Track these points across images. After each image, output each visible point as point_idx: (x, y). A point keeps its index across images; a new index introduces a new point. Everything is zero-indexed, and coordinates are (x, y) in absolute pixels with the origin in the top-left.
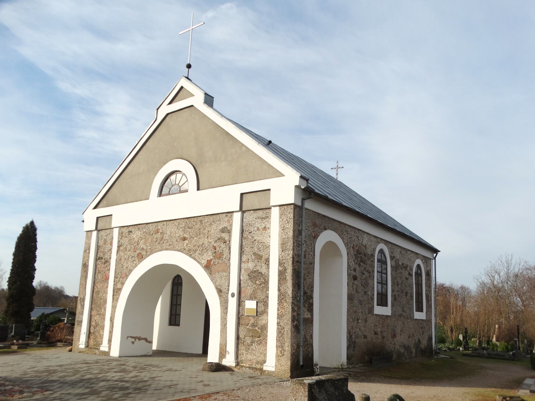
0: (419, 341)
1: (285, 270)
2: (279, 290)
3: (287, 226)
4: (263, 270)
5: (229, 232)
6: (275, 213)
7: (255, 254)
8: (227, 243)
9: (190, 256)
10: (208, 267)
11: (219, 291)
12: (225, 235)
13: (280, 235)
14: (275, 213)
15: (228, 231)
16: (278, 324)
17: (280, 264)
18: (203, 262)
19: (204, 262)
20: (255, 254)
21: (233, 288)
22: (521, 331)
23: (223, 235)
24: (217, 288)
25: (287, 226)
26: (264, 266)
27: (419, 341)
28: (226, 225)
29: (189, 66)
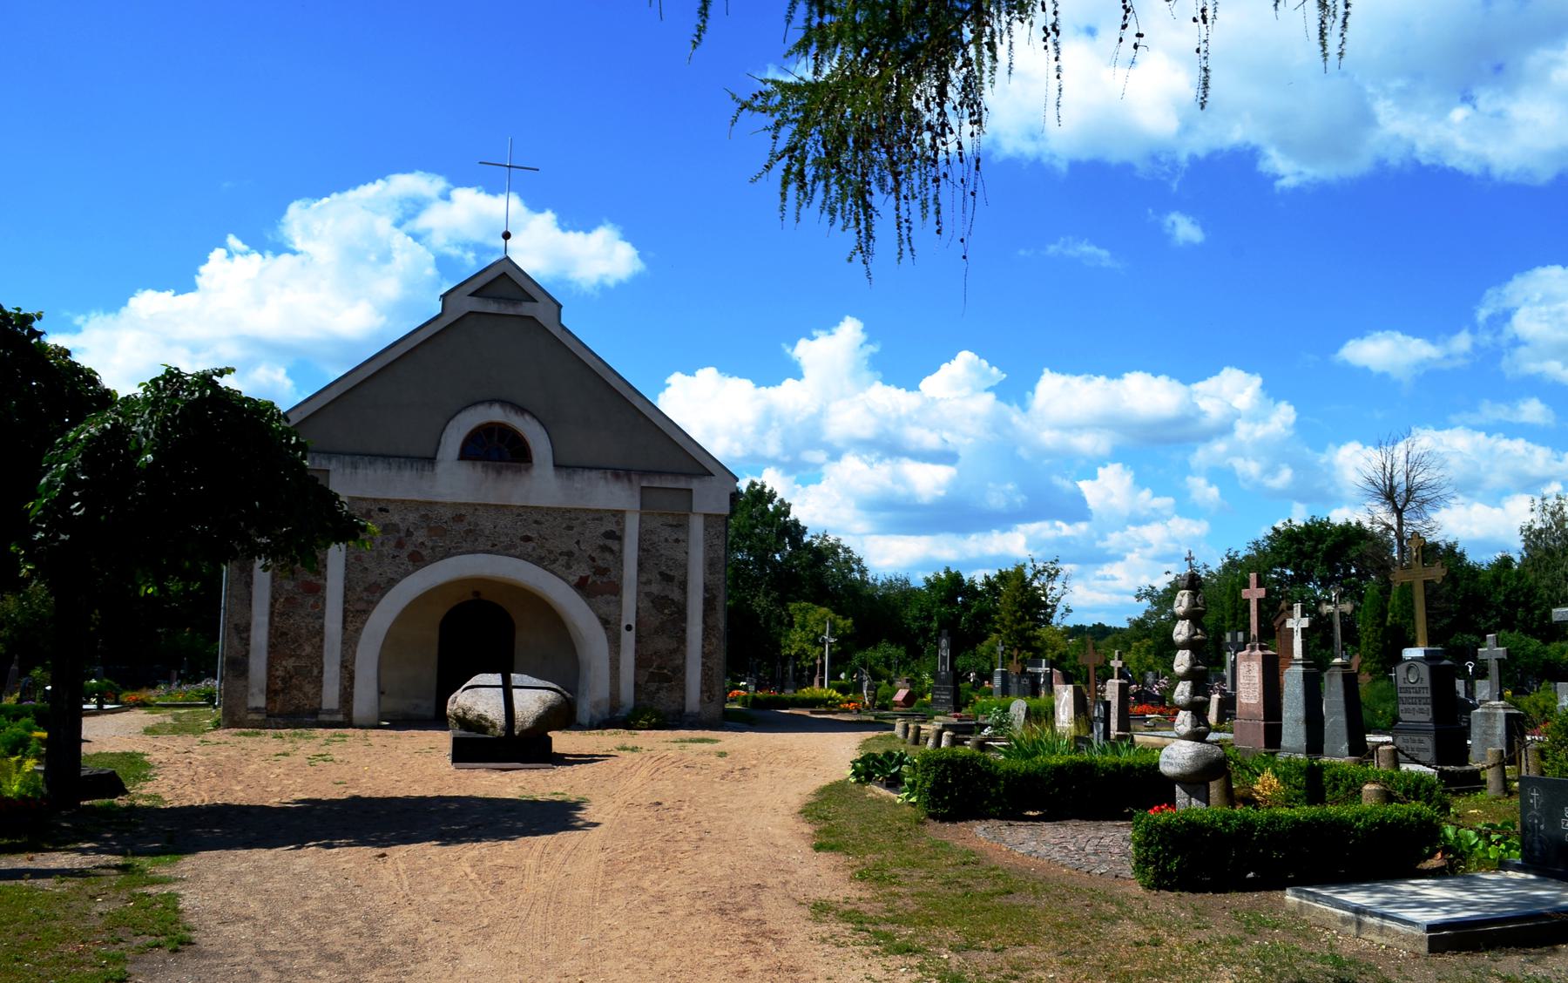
0: (1283, 177)
1: (715, 597)
2: (705, 622)
3: (716, 542)
4: (676, 595)
5: (620, 539)
6: (697, 525)
7: (661, 574)
8: (618, 556)
9: (545, 568)
10: (581, 586)
11: (605, 622)
12: (614, 545)
13: (706, 552)
14: (697, 525)
15: (616, 536)
16: (703, 664)
17: (706, 589)
18: (571, 578)
19: (575, 579)
20: (661, 574)
21: (629, 617)
22: (186, 947)
23: (609, 543)
24: (600, 618)
25: (716, 542)
26: (677, 591)
27: (1283, 177)
28: (614, 528)
29: (507, 236)
